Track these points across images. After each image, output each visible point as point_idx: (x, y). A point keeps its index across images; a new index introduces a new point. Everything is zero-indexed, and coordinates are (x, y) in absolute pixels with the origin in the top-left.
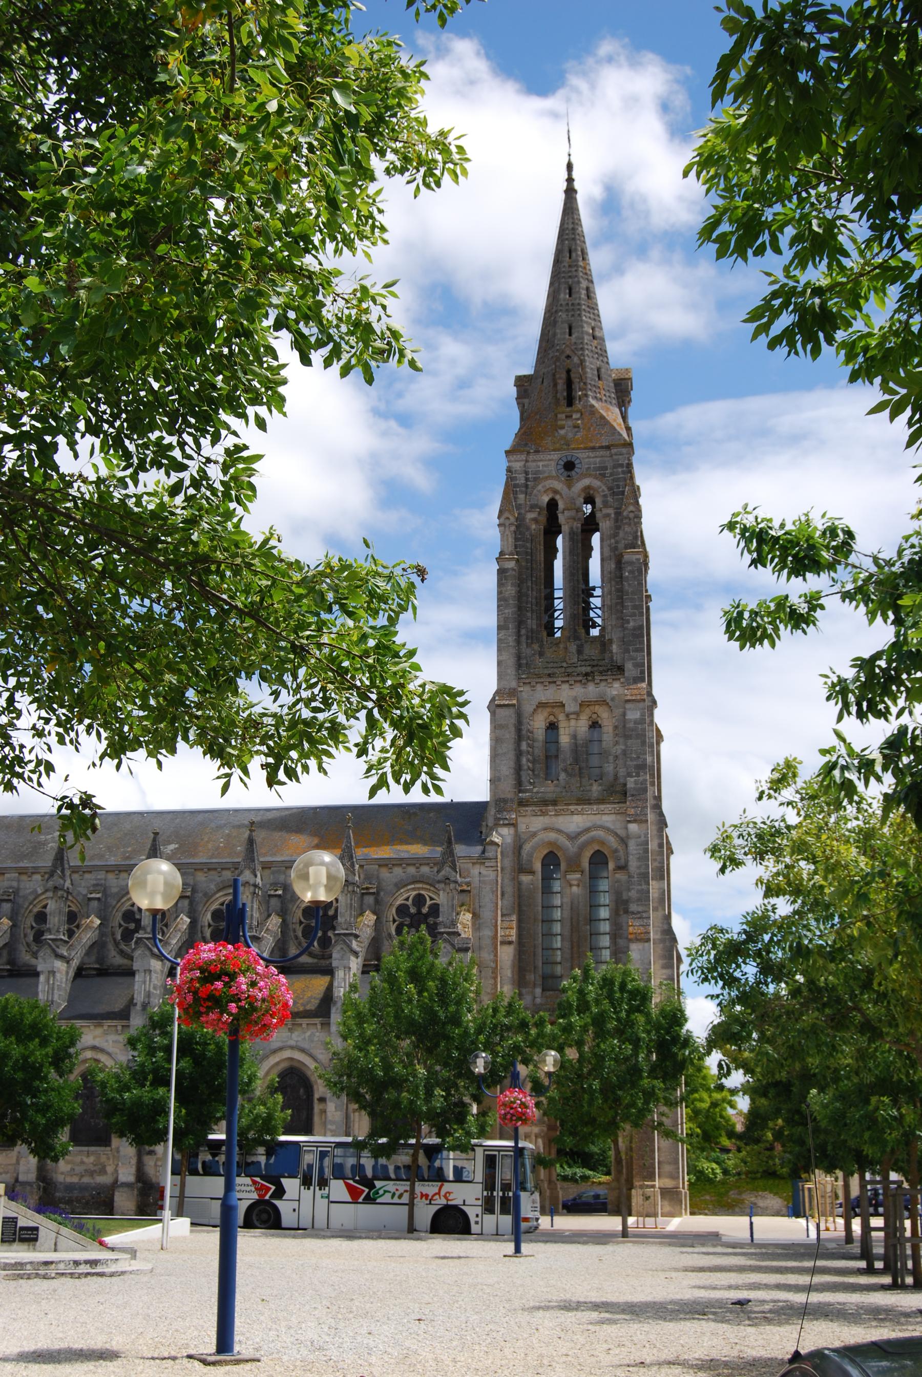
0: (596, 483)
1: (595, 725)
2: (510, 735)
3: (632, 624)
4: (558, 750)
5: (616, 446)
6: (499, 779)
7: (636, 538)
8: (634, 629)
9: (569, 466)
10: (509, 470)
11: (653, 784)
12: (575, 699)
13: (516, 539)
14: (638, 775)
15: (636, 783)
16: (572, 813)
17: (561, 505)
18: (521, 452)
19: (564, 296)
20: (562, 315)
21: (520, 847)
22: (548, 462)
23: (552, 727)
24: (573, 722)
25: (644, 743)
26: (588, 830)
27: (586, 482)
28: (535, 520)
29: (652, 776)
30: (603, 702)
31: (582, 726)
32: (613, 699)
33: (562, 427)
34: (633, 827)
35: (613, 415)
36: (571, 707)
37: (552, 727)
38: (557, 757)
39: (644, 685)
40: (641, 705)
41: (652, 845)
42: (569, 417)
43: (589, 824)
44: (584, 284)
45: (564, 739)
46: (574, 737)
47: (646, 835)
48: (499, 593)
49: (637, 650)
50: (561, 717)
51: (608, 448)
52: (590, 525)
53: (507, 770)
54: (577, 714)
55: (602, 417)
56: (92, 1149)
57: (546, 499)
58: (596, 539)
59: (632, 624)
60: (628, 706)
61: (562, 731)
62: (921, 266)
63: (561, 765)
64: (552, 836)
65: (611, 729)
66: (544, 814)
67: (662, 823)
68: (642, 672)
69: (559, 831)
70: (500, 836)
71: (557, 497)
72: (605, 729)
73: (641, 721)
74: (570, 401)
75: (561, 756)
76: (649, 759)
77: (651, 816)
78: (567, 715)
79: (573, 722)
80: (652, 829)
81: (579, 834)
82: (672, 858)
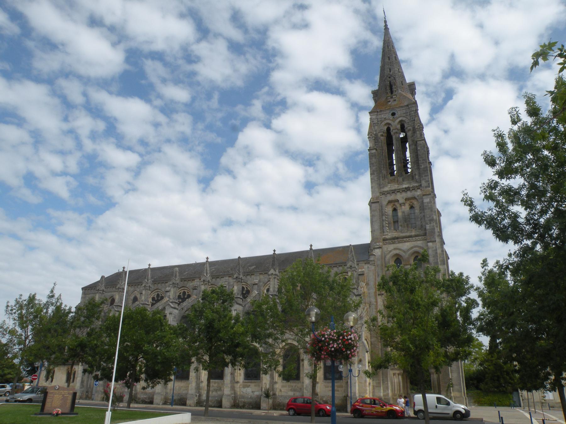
0: (404, 119)
1: (412, 207)
2: (377, 214)
3: (423, 167)
4: (398, 218)
5: (411, 104)
6: (374, 231)
7: (424, 147)
8: (424, 168)
9: (393, 114)
10: (371, 119)
11: (437, 227)
12: (403, 198)
13: (375, 142)
14: (430, 223)
15: (430, 226)
16: (405, 242)
17: (391, 129)
18: (375, 112)
19: (387, 60)
20: (387, 67)
21: (385, 257)
22: (387, 115)
23: (395, 210)
24: (403, 207)
25: (432, 211)
26: (412, 248)
27: (400, 119)
28: (382, 135)
29: (436, 223)
30: (414, 198)
31: (406, 208)
32: (418, 196)
33: (389, 101)
34: (430, 244)
35: (410, 96)
36: (401, 201)
37: (395, 210)
38: (397, 221)
39: (430, 189)
40: (430, 196)
41: (439, 251)
42: (392, 98)
43: (412, 246)
44: (394, 56)
45: (400, 214)
46: (403, 212)
47: (436, 247)
48: (370, 162)
49: (425, 176)
50: (398, 205)
51: (407, 106)
52: (404, 141)
53: (377, 227)
54: (404, 204)
55: (404, 96)
56: (216, 381)
57: (386, 128)
58: (407, 145)
59: (423, 167)
60: (424, 197)
61: (399, 211)
62: (565, 206)
63: (400, 224)
64: (397, 252)
65: (418, 208)
66: (393, 243)
67: (443, 243)
68: (429, 184)
69: (400, 249)
70: (377, 252)
71: (390, 126)
72: (416, 208)
73: (430, 202)
74: (392, 92)
75: (399, 220)
76: (435, 217)
77: (437, 240)
78: (400, 204)
79: (403, 207)
80: (438, 244)
81: (409, 250)
82: (449, 261)
